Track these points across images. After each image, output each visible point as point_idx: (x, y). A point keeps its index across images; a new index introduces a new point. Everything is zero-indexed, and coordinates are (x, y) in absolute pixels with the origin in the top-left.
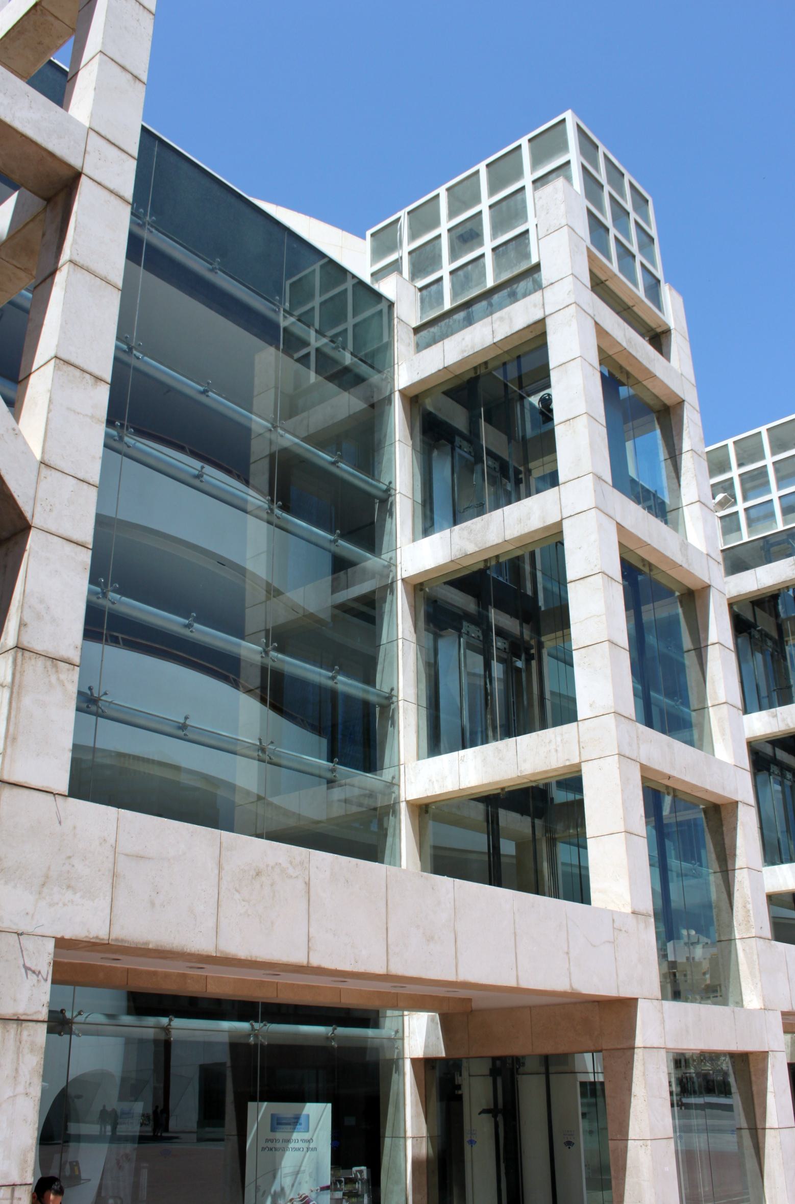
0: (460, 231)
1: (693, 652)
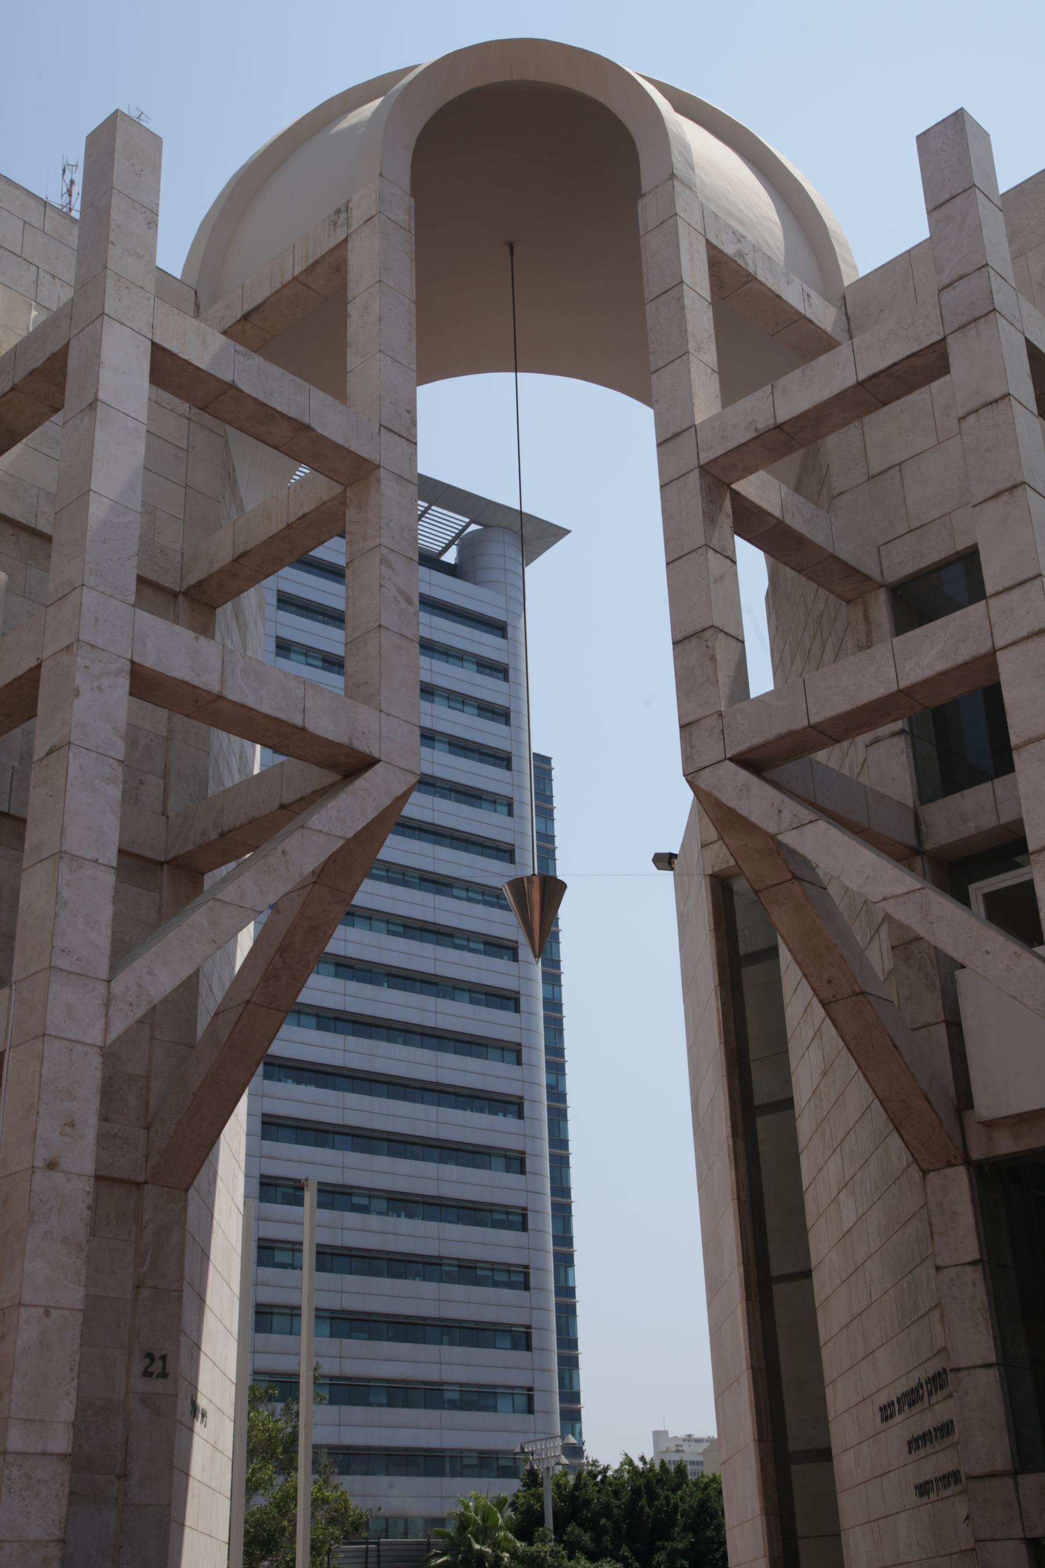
1: (518, 374)
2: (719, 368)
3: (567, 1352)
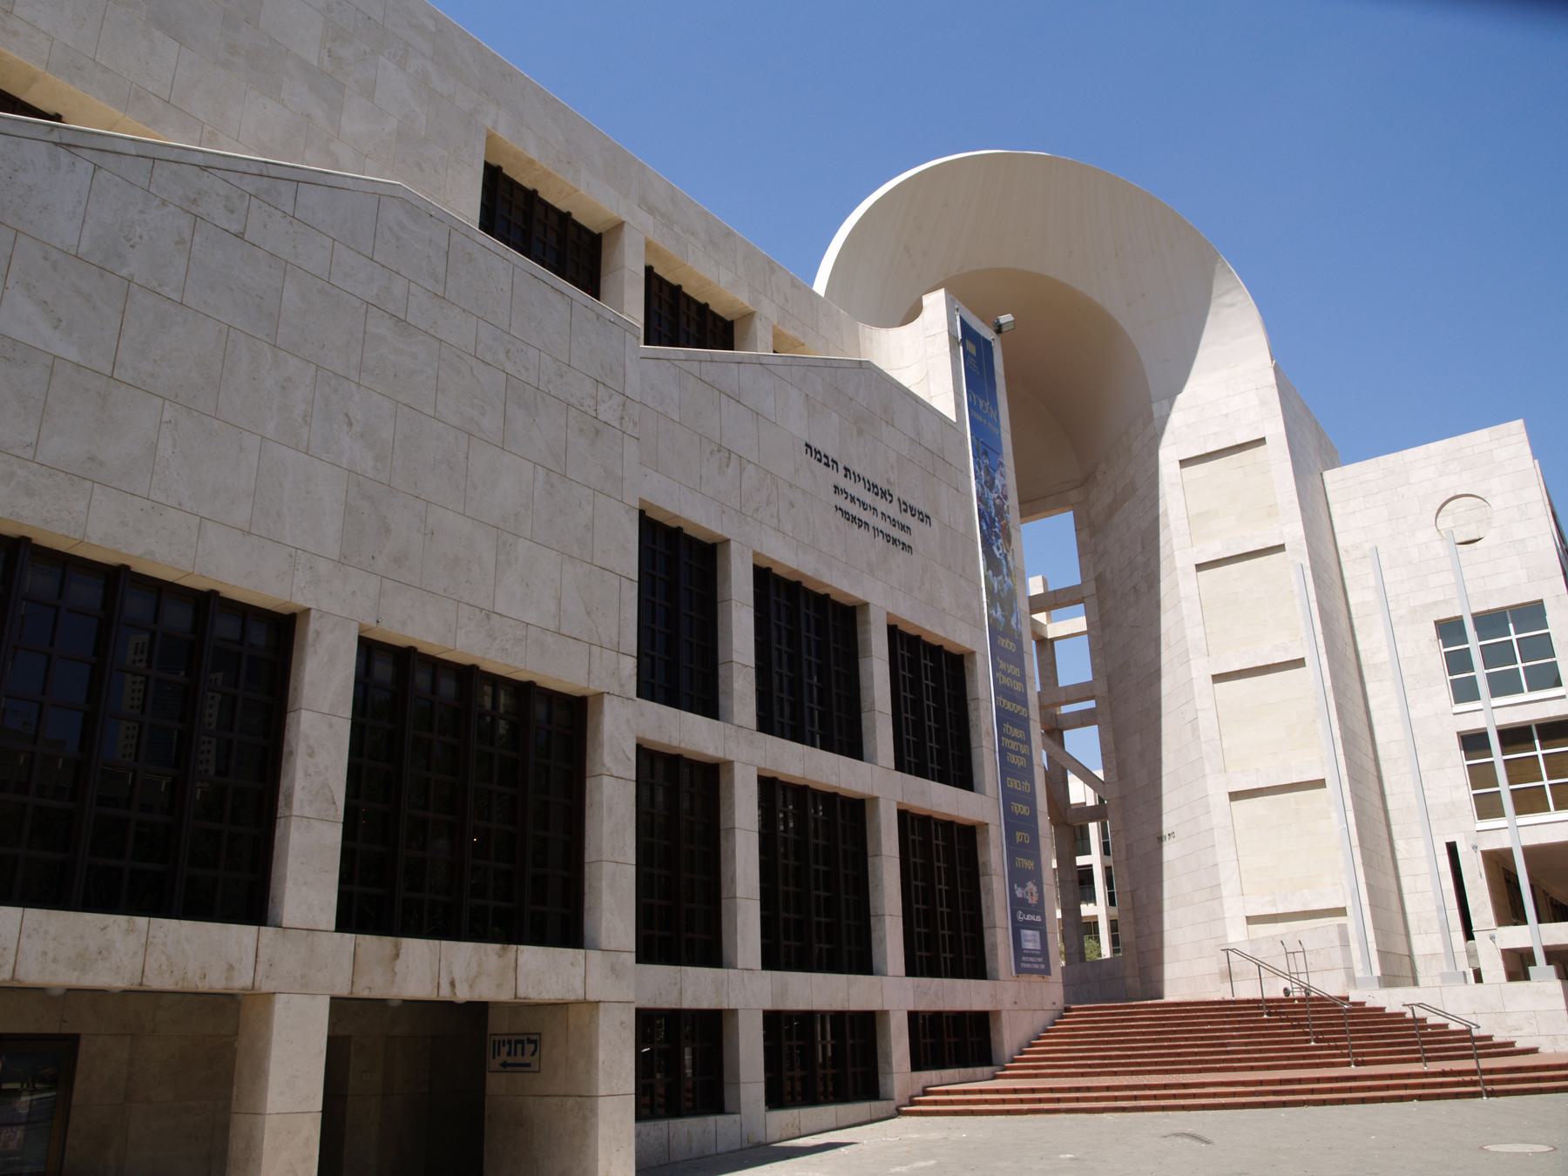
1: (600, 1094)
2: (1105, 776)
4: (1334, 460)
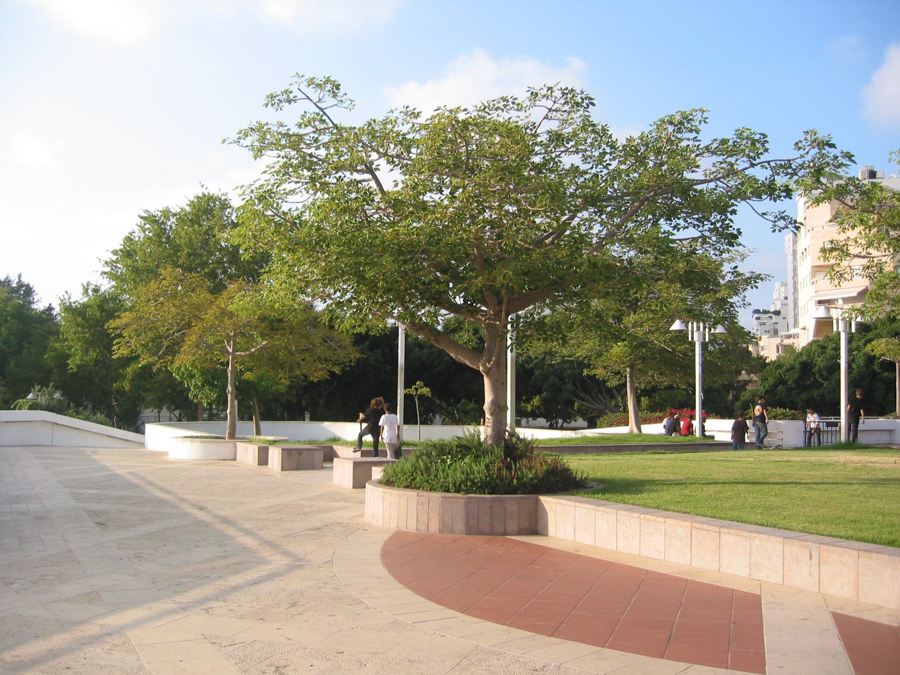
0: (821, 322)
3: (579, 397)
4: (709, 417)
